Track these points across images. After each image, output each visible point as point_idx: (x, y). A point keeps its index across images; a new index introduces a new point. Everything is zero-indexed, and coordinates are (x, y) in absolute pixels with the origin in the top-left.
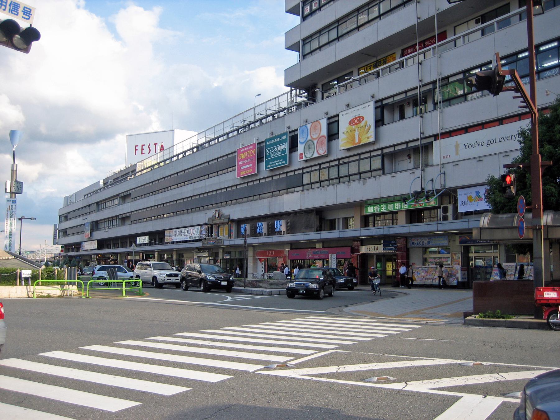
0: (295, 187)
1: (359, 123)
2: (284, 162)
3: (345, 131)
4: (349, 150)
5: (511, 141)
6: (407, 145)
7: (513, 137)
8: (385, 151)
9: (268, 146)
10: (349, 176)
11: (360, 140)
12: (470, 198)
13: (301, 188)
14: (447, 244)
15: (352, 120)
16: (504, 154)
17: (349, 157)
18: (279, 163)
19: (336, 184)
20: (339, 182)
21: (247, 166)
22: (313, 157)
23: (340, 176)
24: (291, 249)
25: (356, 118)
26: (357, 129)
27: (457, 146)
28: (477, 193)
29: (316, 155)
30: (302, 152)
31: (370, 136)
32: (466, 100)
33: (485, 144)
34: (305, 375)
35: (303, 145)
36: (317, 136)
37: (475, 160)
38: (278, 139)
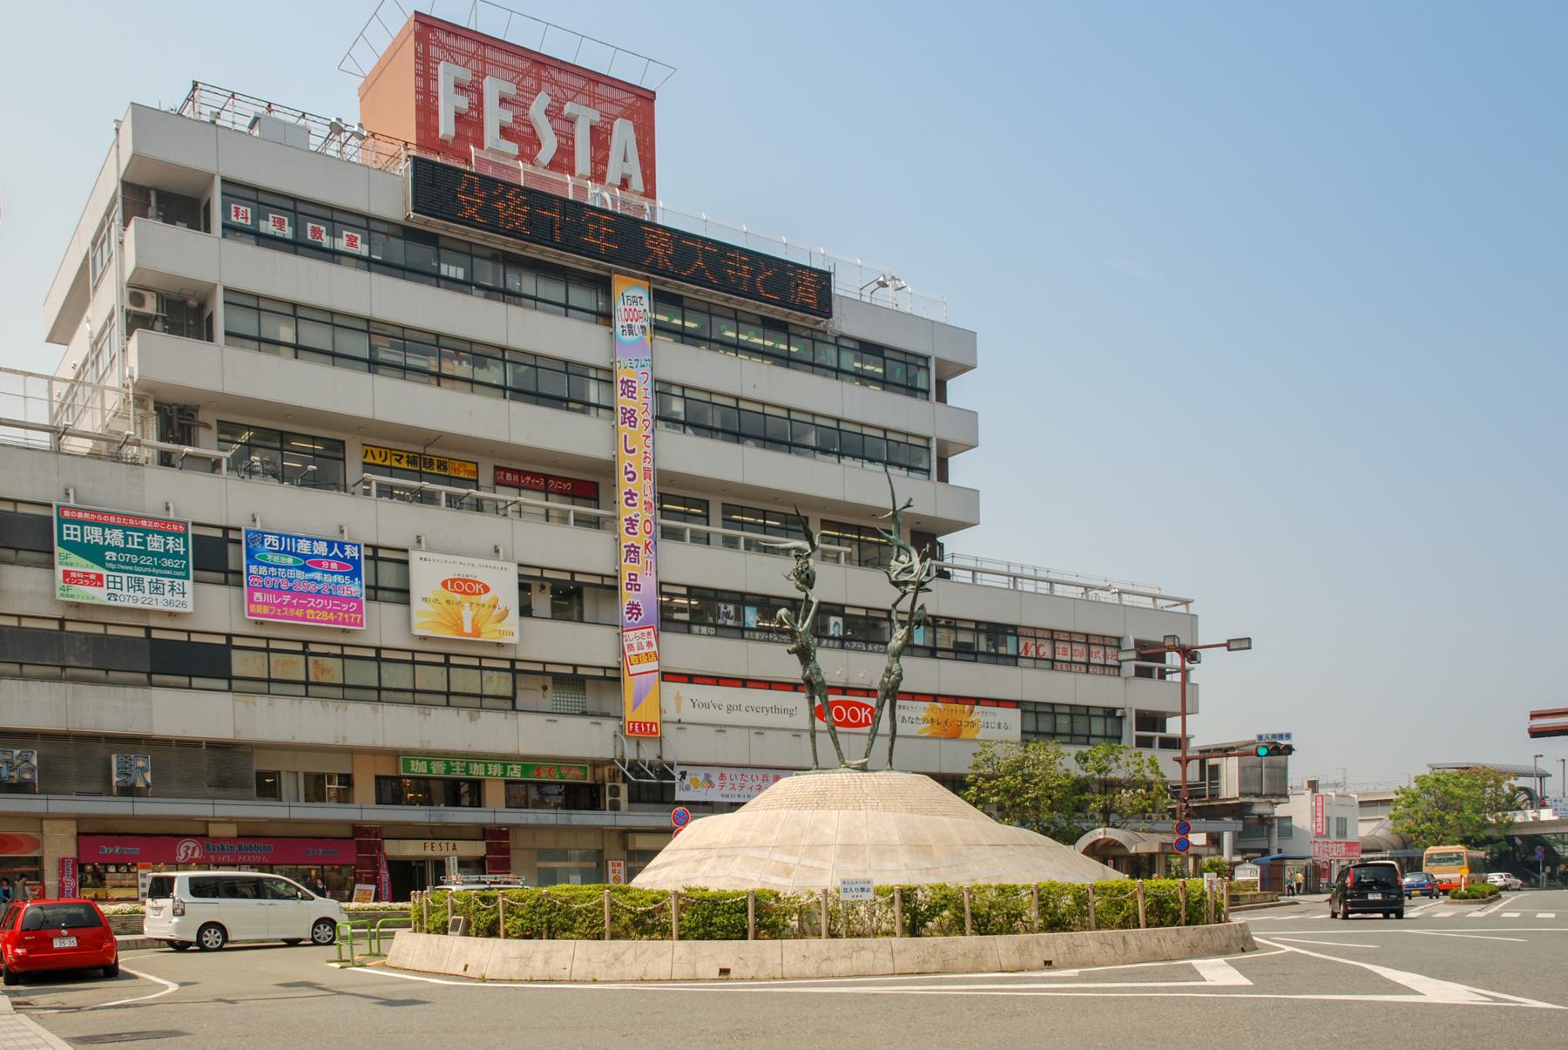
4: (423, 638)
15: (453, 580)
17: (413, 652)
25: (465, 581)
26: (467, 605)
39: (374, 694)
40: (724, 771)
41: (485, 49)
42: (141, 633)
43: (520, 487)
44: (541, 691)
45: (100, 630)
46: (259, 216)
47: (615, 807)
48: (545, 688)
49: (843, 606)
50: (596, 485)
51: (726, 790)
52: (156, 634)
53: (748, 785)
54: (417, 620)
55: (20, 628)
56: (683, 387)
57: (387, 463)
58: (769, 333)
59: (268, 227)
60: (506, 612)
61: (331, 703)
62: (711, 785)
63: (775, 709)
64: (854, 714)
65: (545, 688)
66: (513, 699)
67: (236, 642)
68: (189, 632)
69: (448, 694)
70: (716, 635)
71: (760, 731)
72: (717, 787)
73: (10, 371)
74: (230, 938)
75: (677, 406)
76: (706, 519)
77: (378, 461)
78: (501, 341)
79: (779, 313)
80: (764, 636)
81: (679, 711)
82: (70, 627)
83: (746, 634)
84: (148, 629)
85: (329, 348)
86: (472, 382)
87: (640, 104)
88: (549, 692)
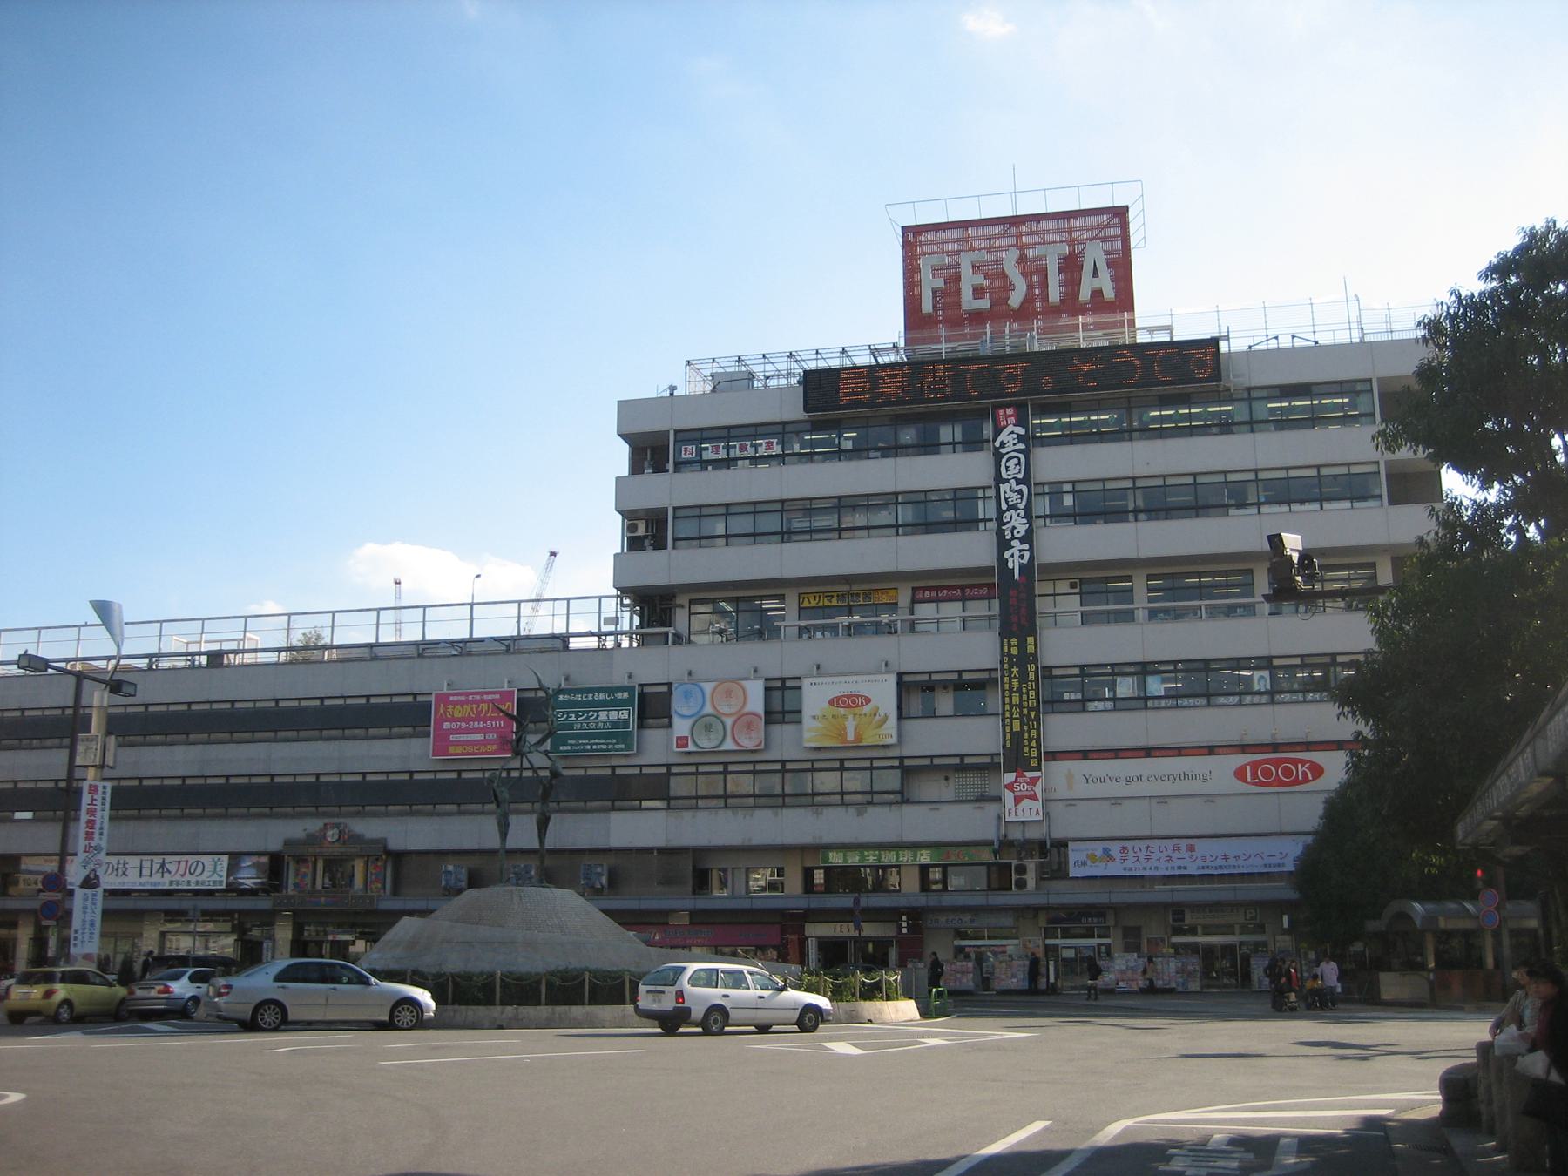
3: (818, 713)
8: (907, 762)
11: (858, 737)
12: (1093, 858)
15: (838, 698)
17: (812, 761)
22: (723, 748)
25: (848, 697)
27: (1070, 776)
28: (1106, 851)
29: (729, 745)
30: (686, 733)
32: (1084, 710)
34: (1388, 1050)
38: (602, 696)
41: (1125, 226)
42: (608, 772)
45: (581, 772)
47: (1022, 885)
49: (1270, 658)
51: (1128, 864)
52: (618, 771)
54: (807, 735)
55: (641, 774)
56: (1074, 482)
60: (886, 717)
61: (740, 812)
62: (1111, 858)
63: (1184, 776)
64: (1287, 772)
66: (901, 792)
67: (674, 770)
68: (641, 766)
69: (725, 797)
70: (1115, 709)
71: (1163, 799)
72: (1118, 861)
74: (291, 1018)
78: (891, 489)
80: (1171, 702)
81: (1070, 787)
83: (1150, 703)
84: (613, 768)
86: (812, 531)
88: (951, 781)
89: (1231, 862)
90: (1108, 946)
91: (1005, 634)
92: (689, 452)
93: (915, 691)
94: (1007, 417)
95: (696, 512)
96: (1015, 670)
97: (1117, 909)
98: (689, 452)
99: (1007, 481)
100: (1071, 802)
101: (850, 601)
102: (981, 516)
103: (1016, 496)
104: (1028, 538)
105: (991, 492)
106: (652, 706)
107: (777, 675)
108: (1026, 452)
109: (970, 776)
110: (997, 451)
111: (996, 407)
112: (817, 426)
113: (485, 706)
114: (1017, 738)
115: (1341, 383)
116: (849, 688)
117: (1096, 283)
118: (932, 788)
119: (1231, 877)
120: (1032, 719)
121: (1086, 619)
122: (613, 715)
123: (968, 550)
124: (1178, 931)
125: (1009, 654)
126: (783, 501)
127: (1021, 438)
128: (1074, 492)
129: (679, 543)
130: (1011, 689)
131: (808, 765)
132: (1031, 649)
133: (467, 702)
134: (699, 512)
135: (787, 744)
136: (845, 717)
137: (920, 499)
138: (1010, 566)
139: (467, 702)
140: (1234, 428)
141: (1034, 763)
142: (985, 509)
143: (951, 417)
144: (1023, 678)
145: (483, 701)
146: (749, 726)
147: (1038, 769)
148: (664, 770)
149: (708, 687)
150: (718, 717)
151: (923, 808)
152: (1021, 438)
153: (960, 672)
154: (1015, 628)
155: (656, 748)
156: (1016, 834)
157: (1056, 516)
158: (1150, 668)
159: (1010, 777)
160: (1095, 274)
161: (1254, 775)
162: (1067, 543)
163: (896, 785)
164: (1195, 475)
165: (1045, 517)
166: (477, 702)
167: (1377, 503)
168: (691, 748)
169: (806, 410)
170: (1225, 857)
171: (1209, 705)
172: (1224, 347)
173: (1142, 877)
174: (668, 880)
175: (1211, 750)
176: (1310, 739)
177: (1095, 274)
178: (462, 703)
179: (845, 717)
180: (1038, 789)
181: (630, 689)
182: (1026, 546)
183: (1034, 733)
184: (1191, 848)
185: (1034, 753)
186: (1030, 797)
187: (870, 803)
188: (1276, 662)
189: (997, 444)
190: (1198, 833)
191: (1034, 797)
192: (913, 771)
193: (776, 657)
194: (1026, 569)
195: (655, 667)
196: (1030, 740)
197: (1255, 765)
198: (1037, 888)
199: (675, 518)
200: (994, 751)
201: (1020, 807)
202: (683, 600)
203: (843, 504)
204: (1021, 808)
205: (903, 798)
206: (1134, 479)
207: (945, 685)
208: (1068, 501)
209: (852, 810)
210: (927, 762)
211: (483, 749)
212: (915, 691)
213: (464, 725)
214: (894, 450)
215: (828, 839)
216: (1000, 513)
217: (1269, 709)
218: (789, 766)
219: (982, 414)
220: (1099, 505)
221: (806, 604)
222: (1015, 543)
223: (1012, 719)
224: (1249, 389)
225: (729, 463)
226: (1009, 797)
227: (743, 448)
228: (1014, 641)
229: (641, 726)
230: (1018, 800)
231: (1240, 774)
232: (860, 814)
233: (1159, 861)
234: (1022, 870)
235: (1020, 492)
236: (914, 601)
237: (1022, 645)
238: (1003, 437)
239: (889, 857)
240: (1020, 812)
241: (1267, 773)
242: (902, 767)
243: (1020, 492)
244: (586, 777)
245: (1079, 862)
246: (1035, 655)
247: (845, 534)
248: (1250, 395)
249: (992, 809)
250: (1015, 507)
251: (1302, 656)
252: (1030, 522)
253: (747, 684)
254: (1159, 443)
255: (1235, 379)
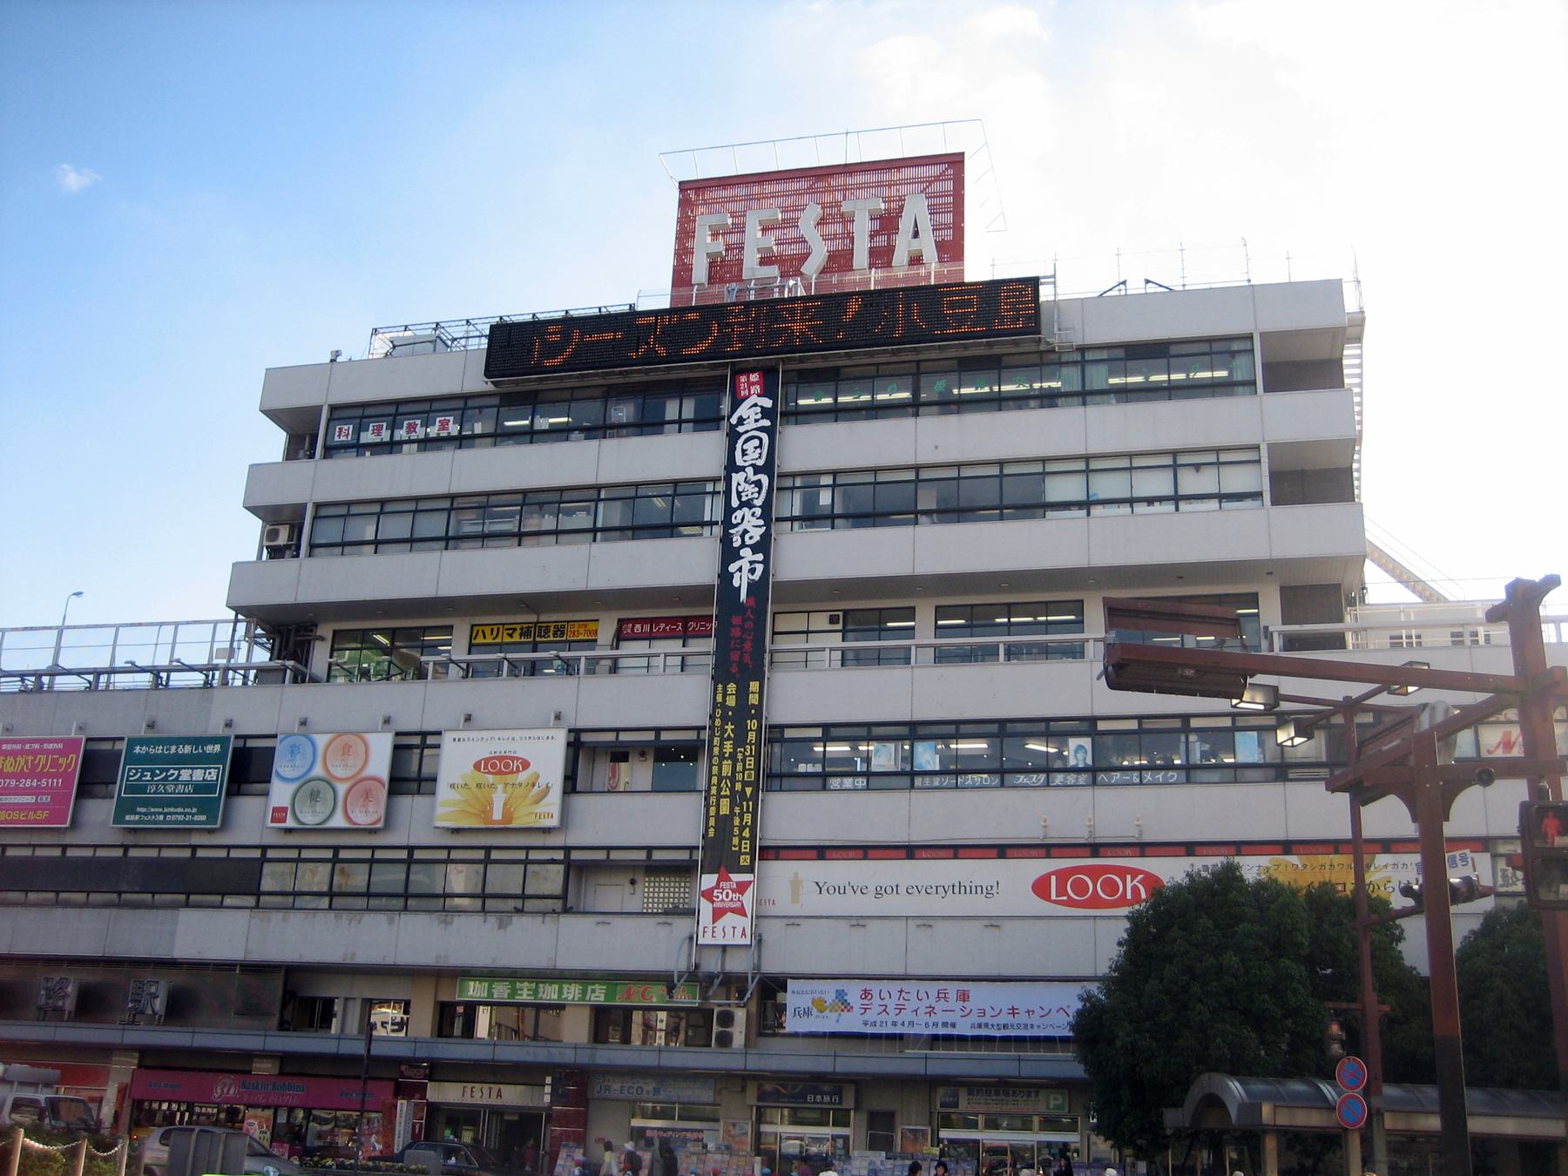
0: (223, 894)
1: (512, 772)
2: (203, 818)
4: (456, 831)
5: (934, 896)
6: (125, 853)
7: (940, 890)
8: (575, 855)
9: (132, 759)
10: (295, 894)
11: (508, 814)
12: (820, 1005)
13: (251, 901)
14: (711, 1100)
15: (487, 760)
16: (920, 922)
17: (449, 848)
18: (181, 818)
19: (175, 906)
20: (330, 908)
21: (30, 799)
23: (488, 891)
24: (140, 1066)
25: (501, 758)
26: (500, 787)
27: (796, 884)
28: (840, 994)
29: (338, 821)
31: (549, 810)
32: (824, 788)
33: (902, 890)
35: (293, 787)
36: (349, 773)
37: (786, 921)
38: (187, 749)
39: (399, 903)
40: (869, 985)
43: (650, 637)
44: (628, 887)
45: (153, 853)
46: (359, 429)
47: (725, 1040)
48: (633, 882)
49: (1093, 720)
50: (1256, 595)
51: (871, 1015)
52: (201, 853)
53: (910, 1006)
55: (228, 858)
56: (835, 473)
57: (498, 640)
58: (966, 376)
59: (367, 437)
61: (345, 915)
62: (847, 1007)
64: (1110, 887)
65: (633, 882)
66: (564, 897)
67: (271, 854)
68: (229, 847)
70: (868, 788)
71: (926, 921)
72: (857, 1010)
73: (25, 629)
75: (282, 539)
76: (1079, 624)
77: (489, 640)
78: (589, 479)
79: (978, 348)
81: (795, 898)
82: (133, 853)
84: (194, 848)
85: (1127, 495)
87: (693, 193)
88: (638, 887)
89: (1022, 1018)
90: (846, 1138)
91: (720, 676)
92: (344, 434)
93: (590, 755)
94: (750, 384)
95: (343, 510)
96: (729, 727)
97: (861, 1083)
98: (344, 434)
99: (743, 469)
100: (793, 920)
101: (536, 631)
102: (707, 518)
103: (752, 489)
104: (763, 546)
105: (721, 487)
106: (248, 766)
107: (415, 727)
108: (770, 431)
109: (664, 881)
110: (732, 428)
111: (736, 373)
112: (510, 401)
113: (43, 758)
114: (724, 823)
115: (1210, 340)
116: (502, 745)
117: (916, 245)
118: (610, 894)
119: (1020, 1040)
120: (747, 799)
121: (848, 659)
122: (198, 775)
123: (685, 562)
124: (947, 1123)
125: (723, 705)
126: (452, 497)
127: (766, 413)
128: (834, 486)
129: (318, 550)
130: (722, 757)
131: (443, 855)
132: (753, 699)
133: (22, 752)
134: (347, 509)
135: (423, 821)
136: (492, 786)
137: (632, 493)
138: (736, 583)
139: (22, 752)
140: (1060, 401)
141: (745, 861)
142: (712, 509)
143: (680, 389)
144: (740, 740)
145: (41, 751)
146: (367, 795)
147: (750, 870)
148: (257, 854)
149: (321, 740)
150: (329, 781)
151: (589, 921)
152: (766, 413)
153: (658, 730)
154: (734, 669)
155: (251, 822)
156: (711, 964)
157: (812, 517)
158: (922, 731)
159: (708, 881)
160: (916, 235)
161: (1061, 890)
162: (813, 555)
163: (556, 887)
164: (1001, 463)
165: (792, 519)
166: (34, 753)
167: (1256, 503)
168: (290, 823)
169: (489, 373)
170: (1013, 1011)
171: (1002, 785)
172: (1045, 294)
173: (901, 1036)
174: (250, 1010)
175: (1002, 851)
176: (1147, 838)
177: (916, 235)
178: (14, 754)
179: (492, 786)
180: (748, 899)
181: (223, 741)
182: (760, 557)
183: (748, 818)
184: (964, 996)
185: (746, 846)
186: (734, 911)
187: (519, 911)
188: (1102, 726)
189: (734, 420)
190: (994, 972)
191: (741, 911)
192: (584, 869)
193: (411, 703)
194: (757, 588)
195: (259, 712)
196: (742, 829)
197: (1063, 875)
198: (747, 1044)
199: (315, 518)
200: (694, 844)
201: (720, 924)
202: (326, 630)
203: (531, 499)
204: (721, 929)
205: (566, 905)
206: (917, 468)
207: (642, 750)
208: (825, 498)
209: (492, 920)
210: (601, 855)
211: (32, 816)
212: (590, 755)
213: (13, 783)
214: (600, 430)
215: (458, 959)
216: (729, 510)
217: (1089, 791)
218: (418, 855)
219: (717, 385)
220: (874, 502)
221: (480, 640)
222: (746, 552)
223: (719, 797)
224: (1082, 349)
225: (392, 447)
226: (706, 908)
227: (412, 428)
228: (732, 688)
229: (231, 793)
230: (718, 914)
231: (1041, 888)
232: (502, 926)
233: (916, 1013)
234: (727, 1019)
235: (758, 484)
236: (619, 637)
237: (742, 694)
238: (743, 411)
239: (550, 993)
240: (719, 933)
241: (1080, 887)
242: (568, 864)
243: (758, 484)
244: (159, 862)
245: (803, 1010)
246: (759, 708)
247: (525, 540)
248: (1083, 355)
249: (682, 925)
250: (749, 504)
251: (1140, 718)
252: (768, 524)
253: (370, 737)
254: (952, 421)
255: (1056, 334)
